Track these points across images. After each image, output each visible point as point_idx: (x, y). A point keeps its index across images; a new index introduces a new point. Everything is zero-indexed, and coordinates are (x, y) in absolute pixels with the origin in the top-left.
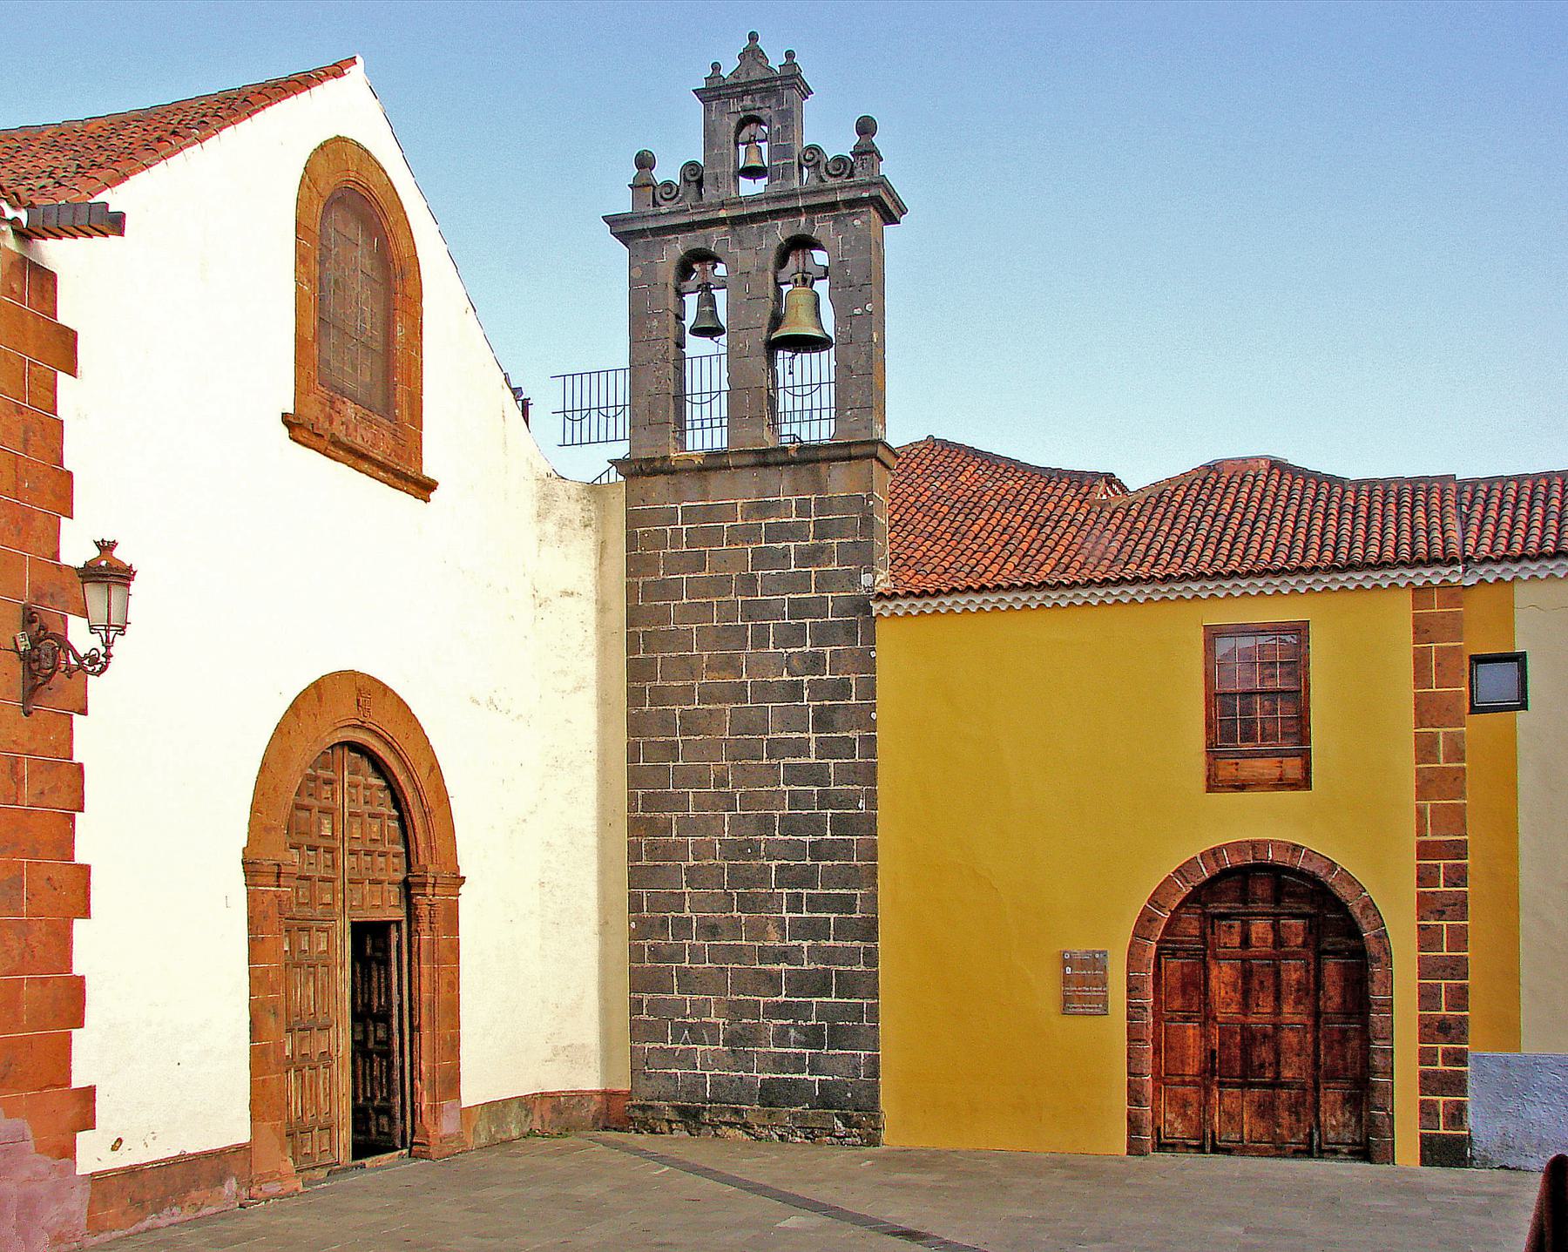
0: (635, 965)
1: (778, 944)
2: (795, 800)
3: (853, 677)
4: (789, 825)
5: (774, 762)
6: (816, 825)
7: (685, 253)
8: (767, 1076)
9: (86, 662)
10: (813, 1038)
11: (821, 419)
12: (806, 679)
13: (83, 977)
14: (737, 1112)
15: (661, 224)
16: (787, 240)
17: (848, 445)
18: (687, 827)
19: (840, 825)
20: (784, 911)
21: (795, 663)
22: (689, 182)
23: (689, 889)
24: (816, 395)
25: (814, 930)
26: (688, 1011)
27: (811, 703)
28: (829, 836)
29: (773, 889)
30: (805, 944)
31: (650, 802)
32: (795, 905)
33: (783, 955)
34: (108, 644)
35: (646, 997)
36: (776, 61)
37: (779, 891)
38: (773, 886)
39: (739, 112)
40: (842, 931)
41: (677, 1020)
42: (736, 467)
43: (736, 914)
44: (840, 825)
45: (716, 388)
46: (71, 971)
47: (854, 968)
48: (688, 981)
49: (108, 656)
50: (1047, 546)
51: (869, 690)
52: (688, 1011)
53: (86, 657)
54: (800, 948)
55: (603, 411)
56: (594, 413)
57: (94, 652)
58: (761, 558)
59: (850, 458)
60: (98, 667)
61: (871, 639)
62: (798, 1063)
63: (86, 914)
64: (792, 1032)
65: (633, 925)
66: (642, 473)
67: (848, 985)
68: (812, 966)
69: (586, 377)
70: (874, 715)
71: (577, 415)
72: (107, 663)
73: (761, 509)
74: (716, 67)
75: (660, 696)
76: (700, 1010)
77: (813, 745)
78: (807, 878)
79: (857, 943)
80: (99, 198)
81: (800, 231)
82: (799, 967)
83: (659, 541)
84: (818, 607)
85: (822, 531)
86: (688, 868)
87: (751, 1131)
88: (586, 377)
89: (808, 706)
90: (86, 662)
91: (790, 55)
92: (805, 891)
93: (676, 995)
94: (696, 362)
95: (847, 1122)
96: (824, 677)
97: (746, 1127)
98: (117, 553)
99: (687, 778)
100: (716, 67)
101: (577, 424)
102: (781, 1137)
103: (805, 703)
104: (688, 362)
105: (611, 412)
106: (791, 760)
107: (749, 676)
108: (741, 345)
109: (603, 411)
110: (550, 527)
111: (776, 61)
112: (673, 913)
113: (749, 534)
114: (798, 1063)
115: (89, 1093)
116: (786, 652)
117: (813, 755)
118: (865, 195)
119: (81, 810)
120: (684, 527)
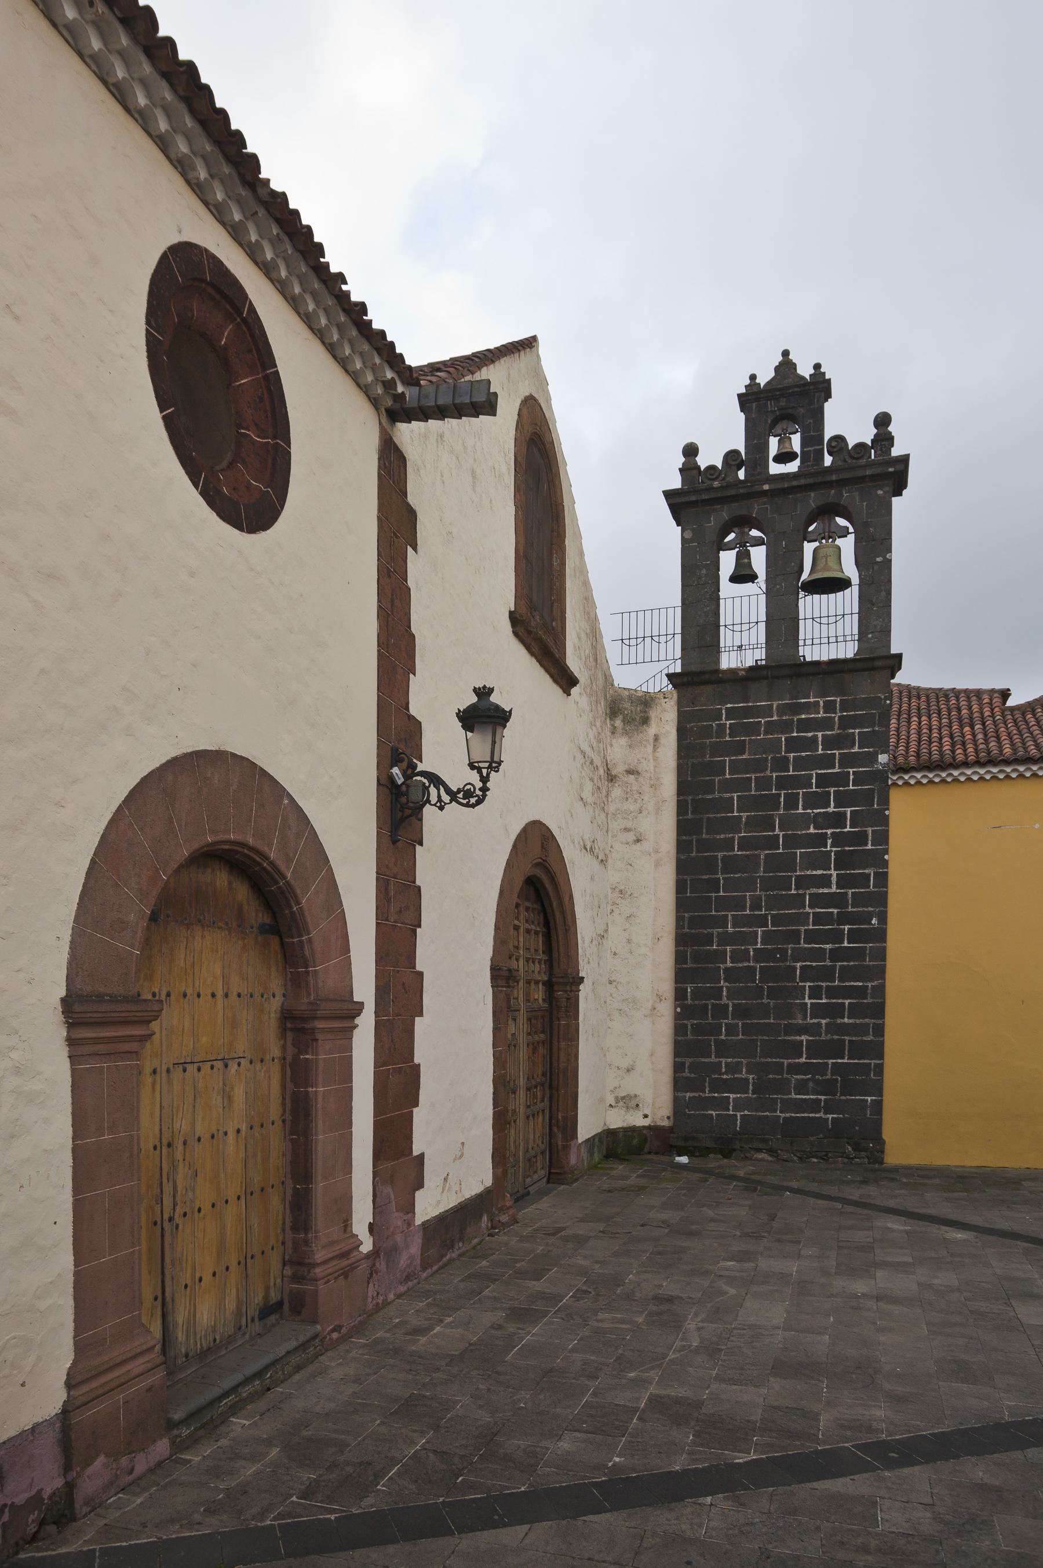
0: (679, 1038)
1: (800, 1022)
2: (818, 919)
3: (870, 830)
4: (811, 936)
5: (801, 892)
6: (836, 936)
7: (729, 519)
8: (788, 1115)
9: (461, 795)
10: (827, 1088)
11: (813, 644)
12: (829, 832)
13: (419, 1065)
14: (765, 1141)
15: (713, 496)
16: (818, 508)
17: (873, 659)
18: (726, 939)
19: (853, 936)
20: (807, 998)
21: (820, 820)
22: (731, 465)
23: (727, 984)
24: (840, 624)
25: (835, 1011)
26: (724, 1070)
27: (834, 849)
28: (846, 944)
29: (798, 983)
30: (823, 1022)
31: (693, 922)
32: (815, 993)
33: (805, 1029)
34: (485, 780)
35: (688, 1061)
36: (805, 370)
37: (803, 984)
38: (798, 981)
39: (775, 411)
40: (854, 1011)
41: (713, 1076)
42: (772, 677)
43: (765, 1001)
44: (853, 936)
45: (754, 619)
46: (413, 1061)
47: (865, 1038)
48: (723, 1049)
49: (485, 790)
50: (990, 737)
51: (883, 838)
52: (724, 1070)
53: (459, 791)
54: (819, 1024)
55: (656, 639)
56: (648, 640)
57: (468, 787)
58: (793, 744)
59: (873, 669)
60: (473, 800)
61: (885, 801)
62: (814, 1106)
63: (421, 1014)
64: (811, 1084)
65: (679, 1010)
66: (692, 684)
67: (857, 1050)
68: (829, 1037)
69: (663, 611)
70: (886, 857)
71: (633, 642)
72: (484, 796)
73: (796, 709)
74: (753, 377)
75: (704, 846)
76: (733, 1068)
77: (834, 879)
78: (827, 974)
79: (867, 1020)
80: (478, 376)
81: (830, 500)
82: (817, 1038)
83: (706, 732)
84: (841, 779)
85: (845, 723)
86: (726, 970)
87: (775, 1154)
88: (656, 612)
89: (831, 851)
90: (461, 795)
91: (817, 367)
92: (824, 984)
93: (713, 1059)
94: (729, 602)
95: (857, 1148)
96: (845, 830)
97: (771, 1151)
98: (494, 698)
99: (724, 904)
100: (753, 377)
101: (633, 649)
102: (800, 1158)
103: (829, 849)
104: (722, 602)
105: (663, 639)
106: (814, 890)
107: (781, 830)
108: (778, 587)
109: (656, 639)
110: (618, 723)
111: (805, 370)
112: (712, 1001)
113: (786, 727)
114: (814, 1106)
115: (421, 1157)
116: (813, 812)
117: (834, 886)
118: (891, 470)
119: (420, 926)
120: (728, 722)
